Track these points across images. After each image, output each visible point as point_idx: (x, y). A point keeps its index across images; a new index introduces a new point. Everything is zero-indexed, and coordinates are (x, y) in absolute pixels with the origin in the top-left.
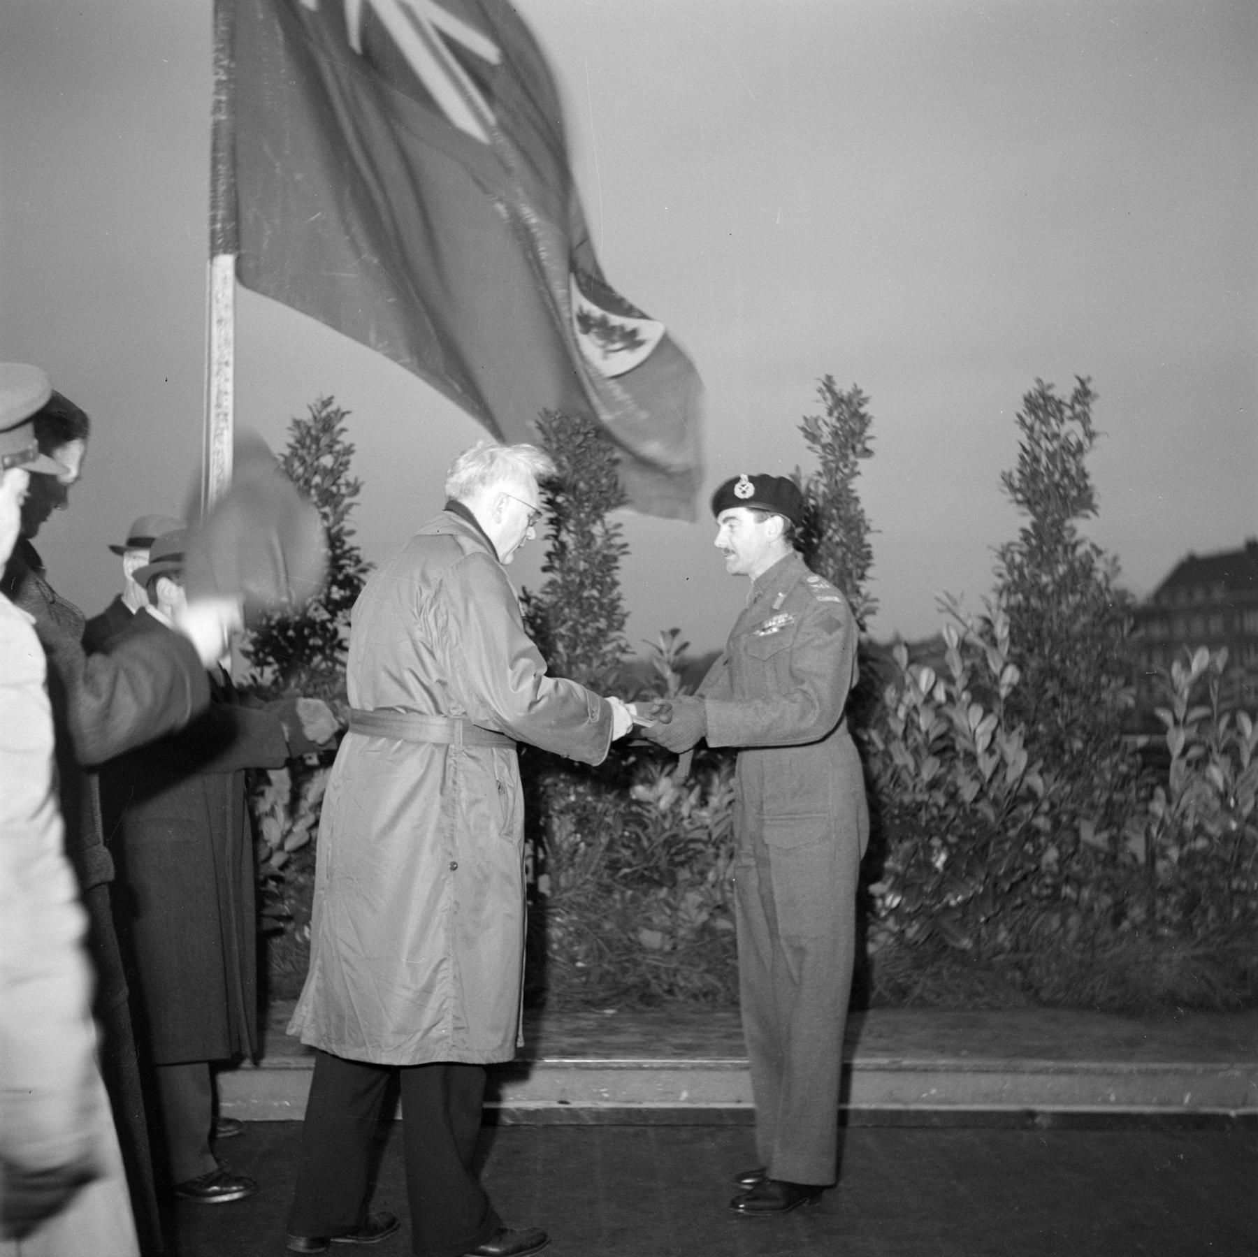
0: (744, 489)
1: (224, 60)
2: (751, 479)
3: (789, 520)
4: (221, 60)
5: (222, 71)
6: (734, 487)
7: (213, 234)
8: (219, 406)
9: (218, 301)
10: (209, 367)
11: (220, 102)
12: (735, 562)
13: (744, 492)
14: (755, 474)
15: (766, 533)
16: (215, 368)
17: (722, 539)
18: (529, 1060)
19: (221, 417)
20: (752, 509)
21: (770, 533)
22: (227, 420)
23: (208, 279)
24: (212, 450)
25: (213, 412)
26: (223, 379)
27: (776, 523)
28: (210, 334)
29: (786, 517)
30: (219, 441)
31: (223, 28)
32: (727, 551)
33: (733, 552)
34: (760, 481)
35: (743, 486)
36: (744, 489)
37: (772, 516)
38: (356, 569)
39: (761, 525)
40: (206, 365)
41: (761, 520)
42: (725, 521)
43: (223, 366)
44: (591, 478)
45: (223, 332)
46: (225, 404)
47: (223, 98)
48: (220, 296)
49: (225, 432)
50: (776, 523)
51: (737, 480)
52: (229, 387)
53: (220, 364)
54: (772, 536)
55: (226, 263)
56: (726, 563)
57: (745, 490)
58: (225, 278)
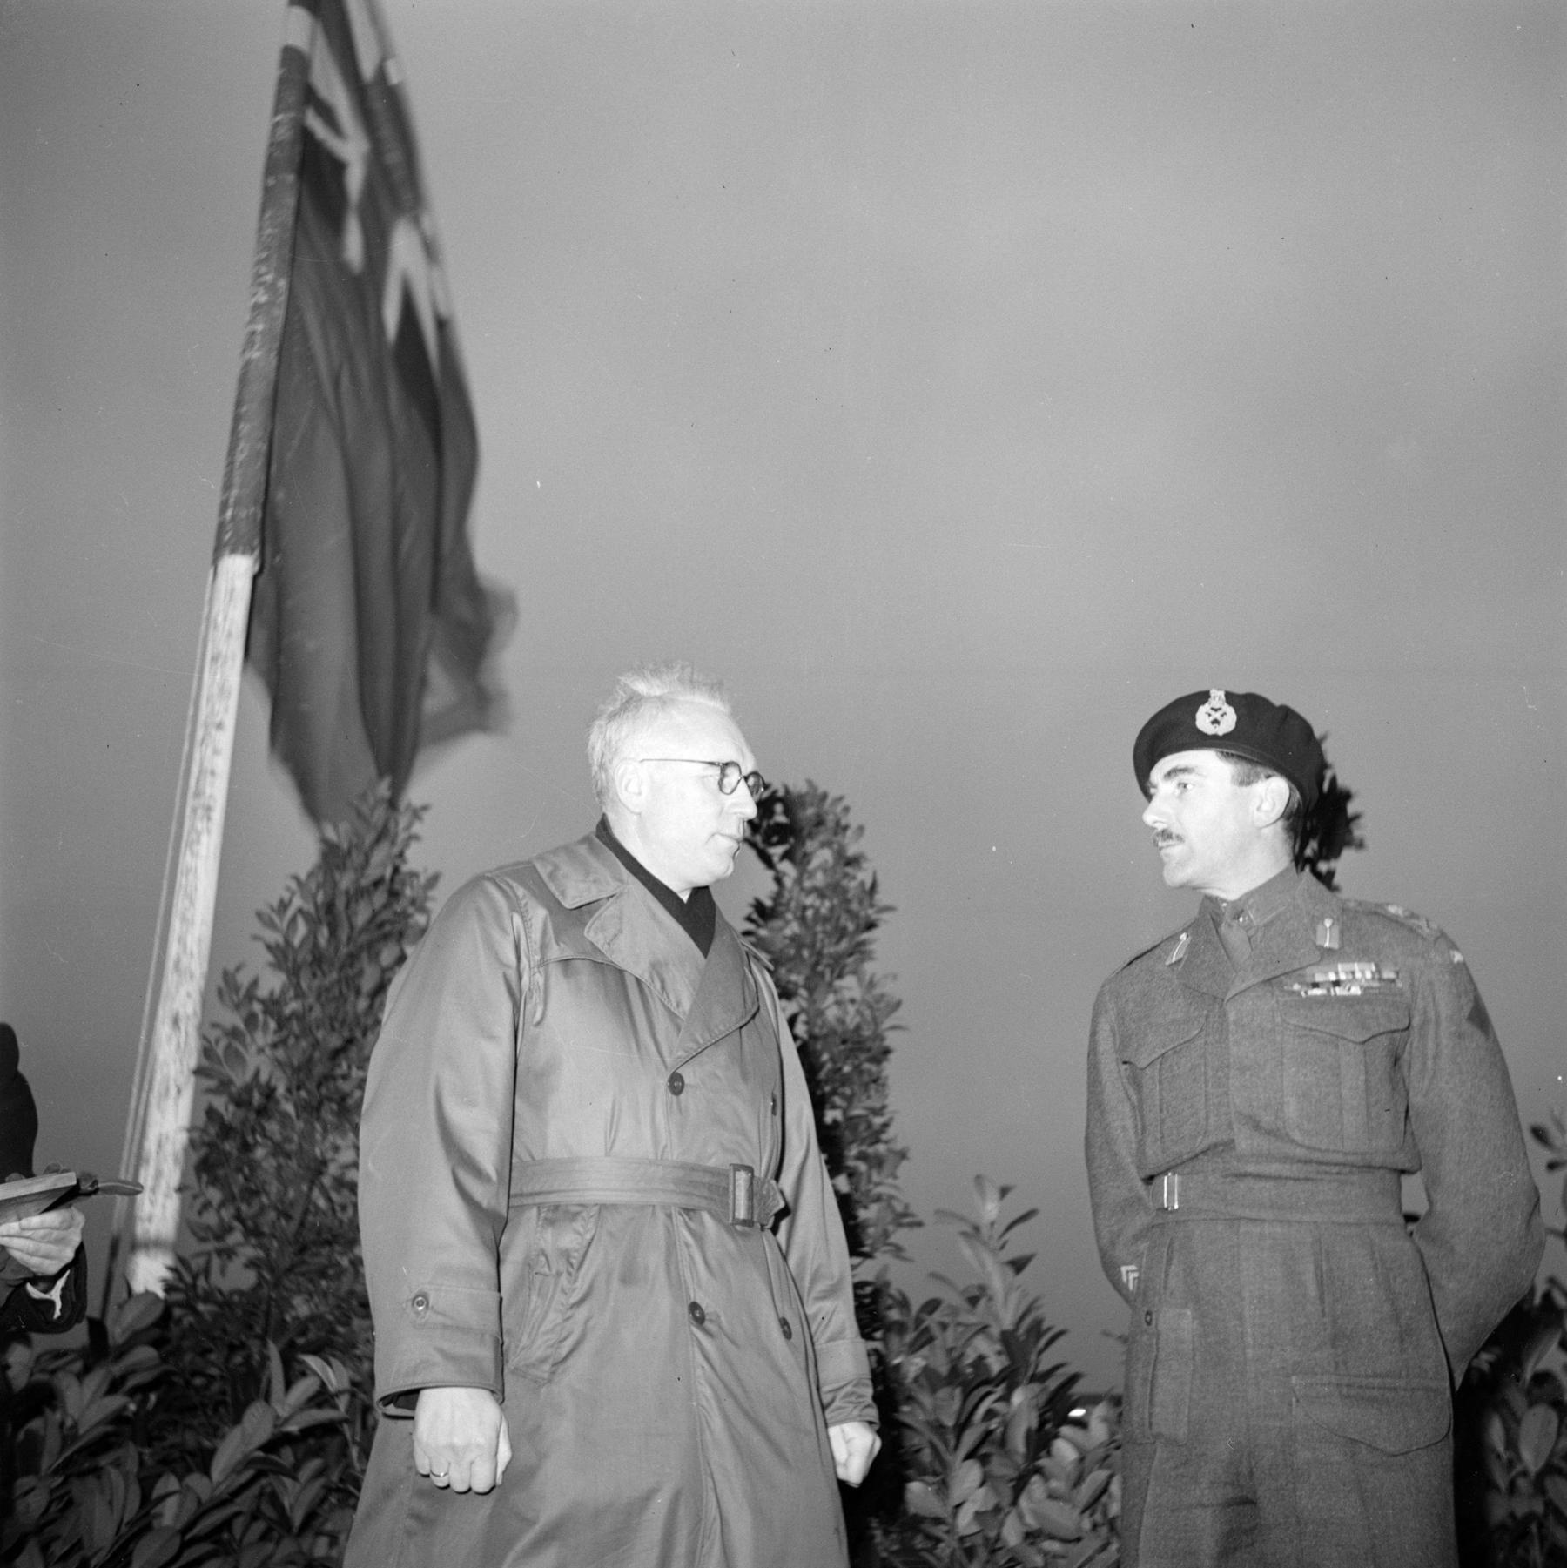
0: (1217, 715)
1: (266, 274)
2: (1230, 698)
3: (1297, 795)
4: (261, 276)
5: (261, 290)
6: (1196, 711)
7: (221, 528)
8: (198, 794)
9: (216, 627)
10: (193, 732)
11: (253, 333)
12: (1182, 864)
13: (1216, 722)
14: (1240, 690)
15: (1253, 808)
16: (200, 733)
17: (1154, 815)
18: (261, 1454)
19: (200, 812)
20: (1227, 756)
21: (1259, 809)
22: (209, 819)
23: (207, 596)
24: (182, 867)
25: (190, 802)
26: (209, 751)
27: (1274, 793)
28: (201, 679)
29: (1293, 786)
30: (192, 853)
31: (268, 231)
32: (1166, 835)
33: (1180, 838)
34: (1246, 704)
35: (1216, 710)
36: (1217, 715)
37: (1268, 777)
38: (312, 1085)
39: (1245, 789)
40: (188, 731)
41: (1245, 781)
42: (1170, 774)
43: (213, 731)
44: (207, 1387)
45: (218, 676)
46: (208, 791)
47: (260, 327)
48: (220, 619)
49: (204, 839)
50: (1274, 793)
51: (1203, 697)
52: (222, 764)
53: (206, 726)
54: (1262, 815)
55: (238, 569)
56: (1160, 864)
57: (1217, 718)
58: (233, 590)
